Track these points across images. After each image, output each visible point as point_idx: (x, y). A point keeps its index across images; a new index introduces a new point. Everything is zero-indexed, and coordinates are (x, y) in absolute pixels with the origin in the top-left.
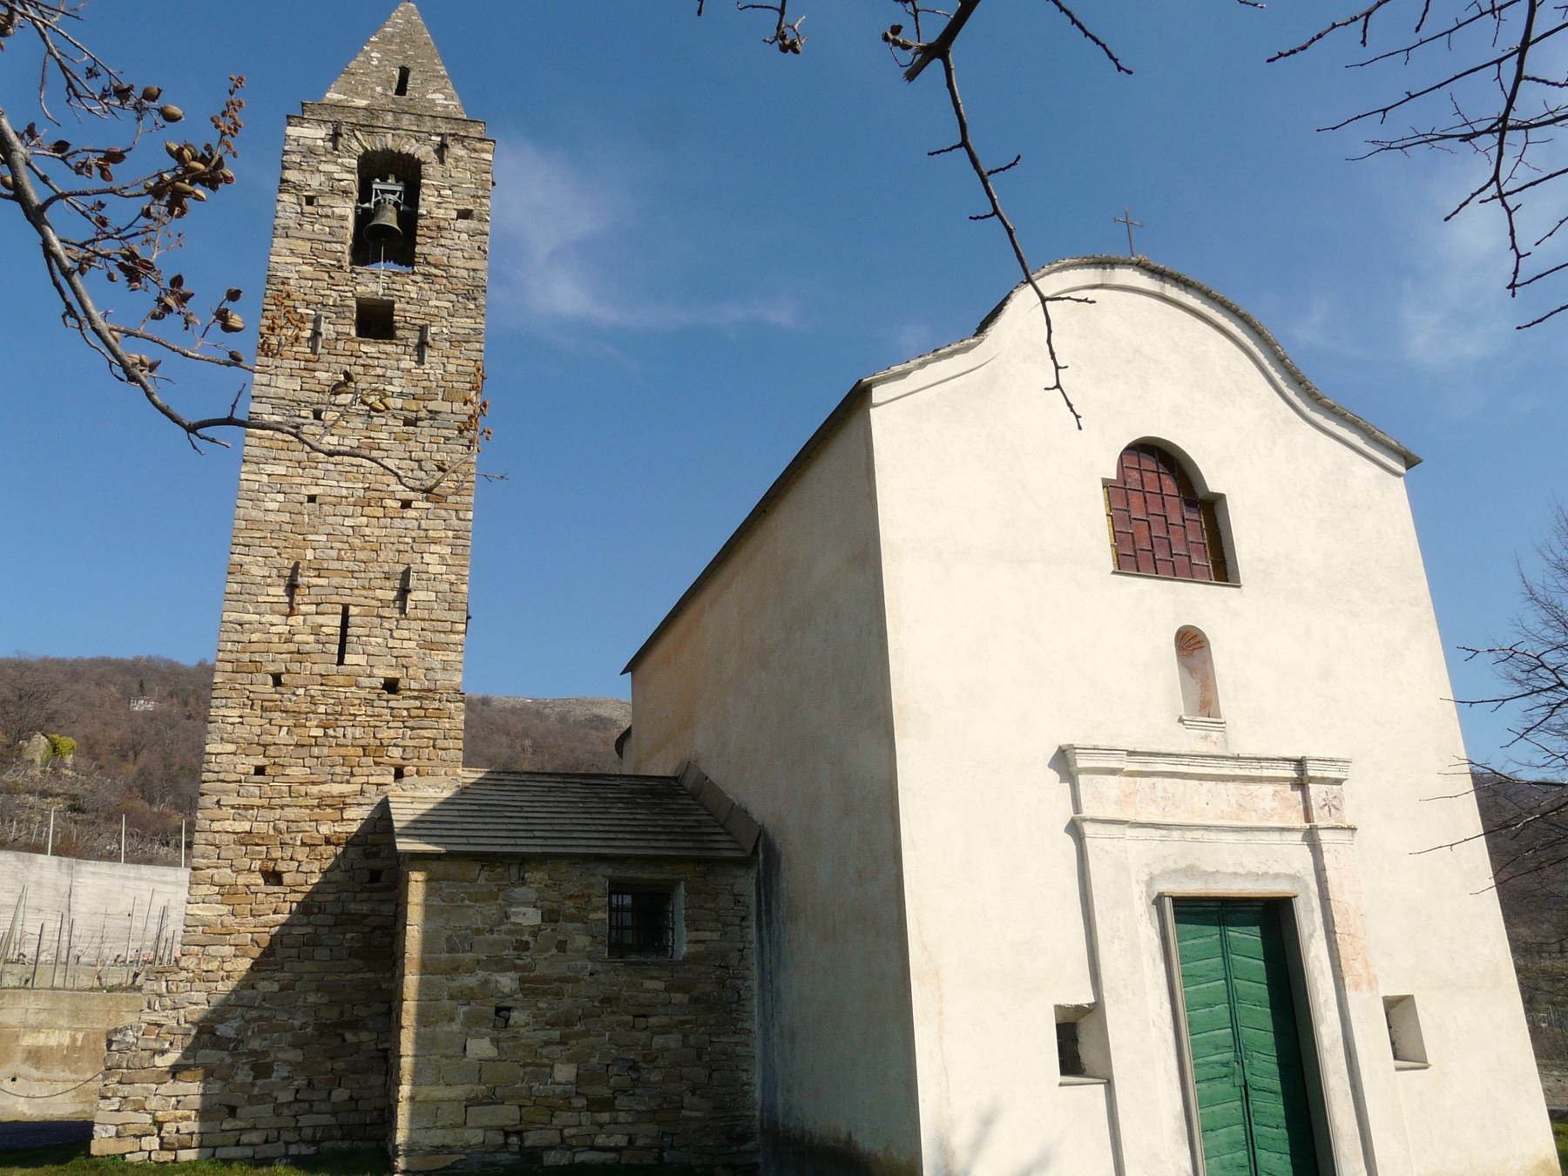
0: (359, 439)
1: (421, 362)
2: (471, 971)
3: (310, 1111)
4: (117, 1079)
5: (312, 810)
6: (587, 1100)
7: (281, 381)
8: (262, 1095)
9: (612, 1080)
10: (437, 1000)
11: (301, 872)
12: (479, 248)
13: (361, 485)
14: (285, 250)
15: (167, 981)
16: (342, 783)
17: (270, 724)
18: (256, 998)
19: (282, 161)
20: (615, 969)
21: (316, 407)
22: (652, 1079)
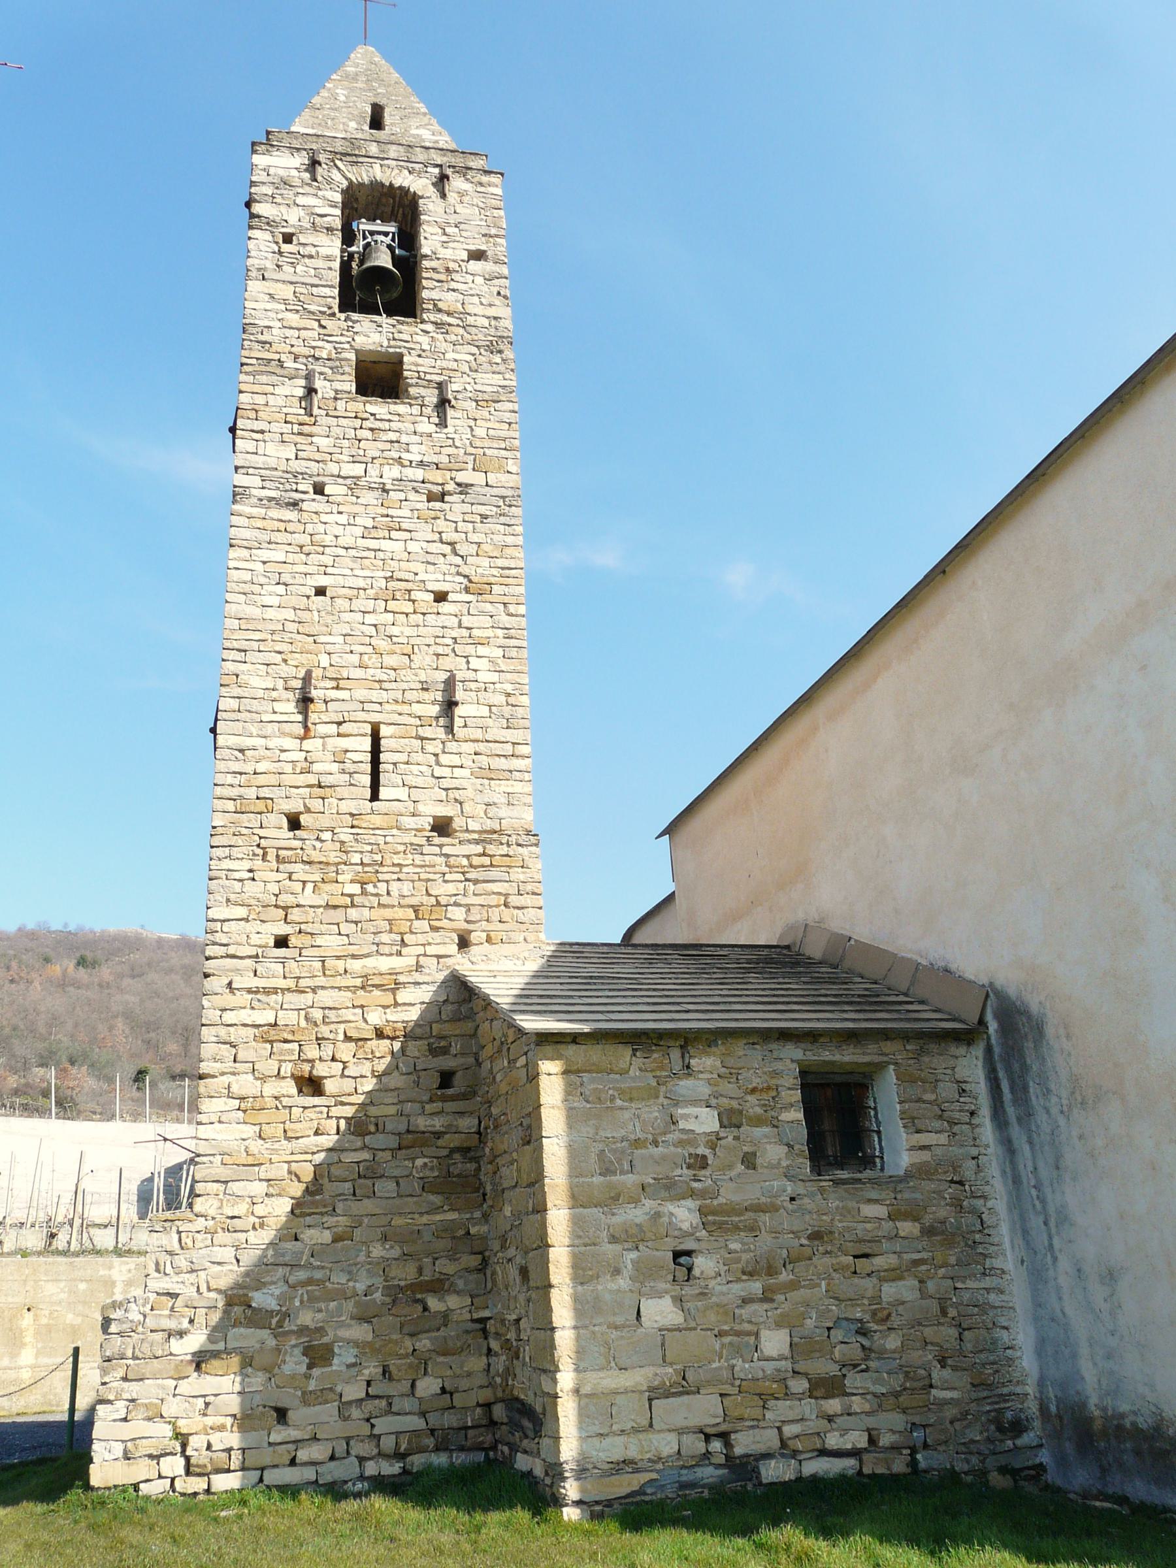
0: (373, 518)
1: (443, 423)
2: (636, 1201)
3: (389, 1411)
4: (121, 1373)
5: (354, 993)
6: (809, 1380)
7: (271, 449)
8: (322, 1390)
9: (836, 1351)
10: (594, 1245)
11: (348, 1077)
12: (499, 293)
13: (382, 574)
14: (262, 295)
15: (179, 1233)
16: (391, 955)
17: (290, 880)
18: (303, 1253)
19: (250, 194)
20: (822, 1190)
21: (316, 479)
22: (888, 1347)
